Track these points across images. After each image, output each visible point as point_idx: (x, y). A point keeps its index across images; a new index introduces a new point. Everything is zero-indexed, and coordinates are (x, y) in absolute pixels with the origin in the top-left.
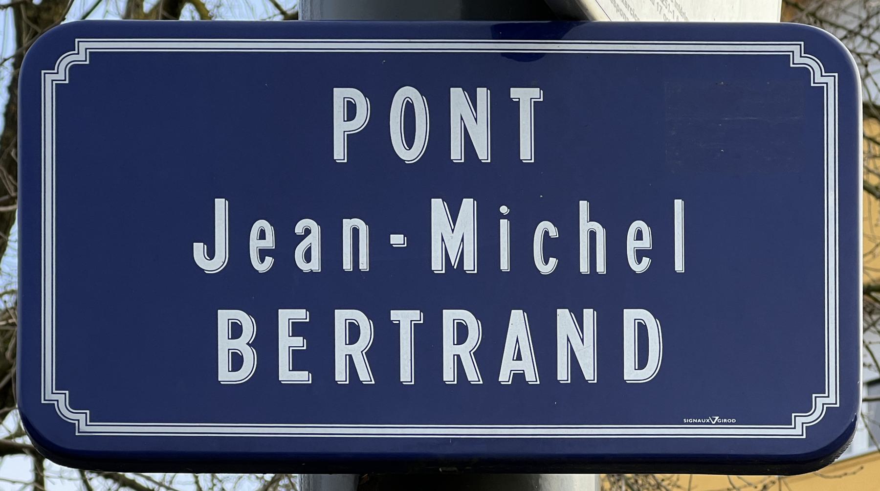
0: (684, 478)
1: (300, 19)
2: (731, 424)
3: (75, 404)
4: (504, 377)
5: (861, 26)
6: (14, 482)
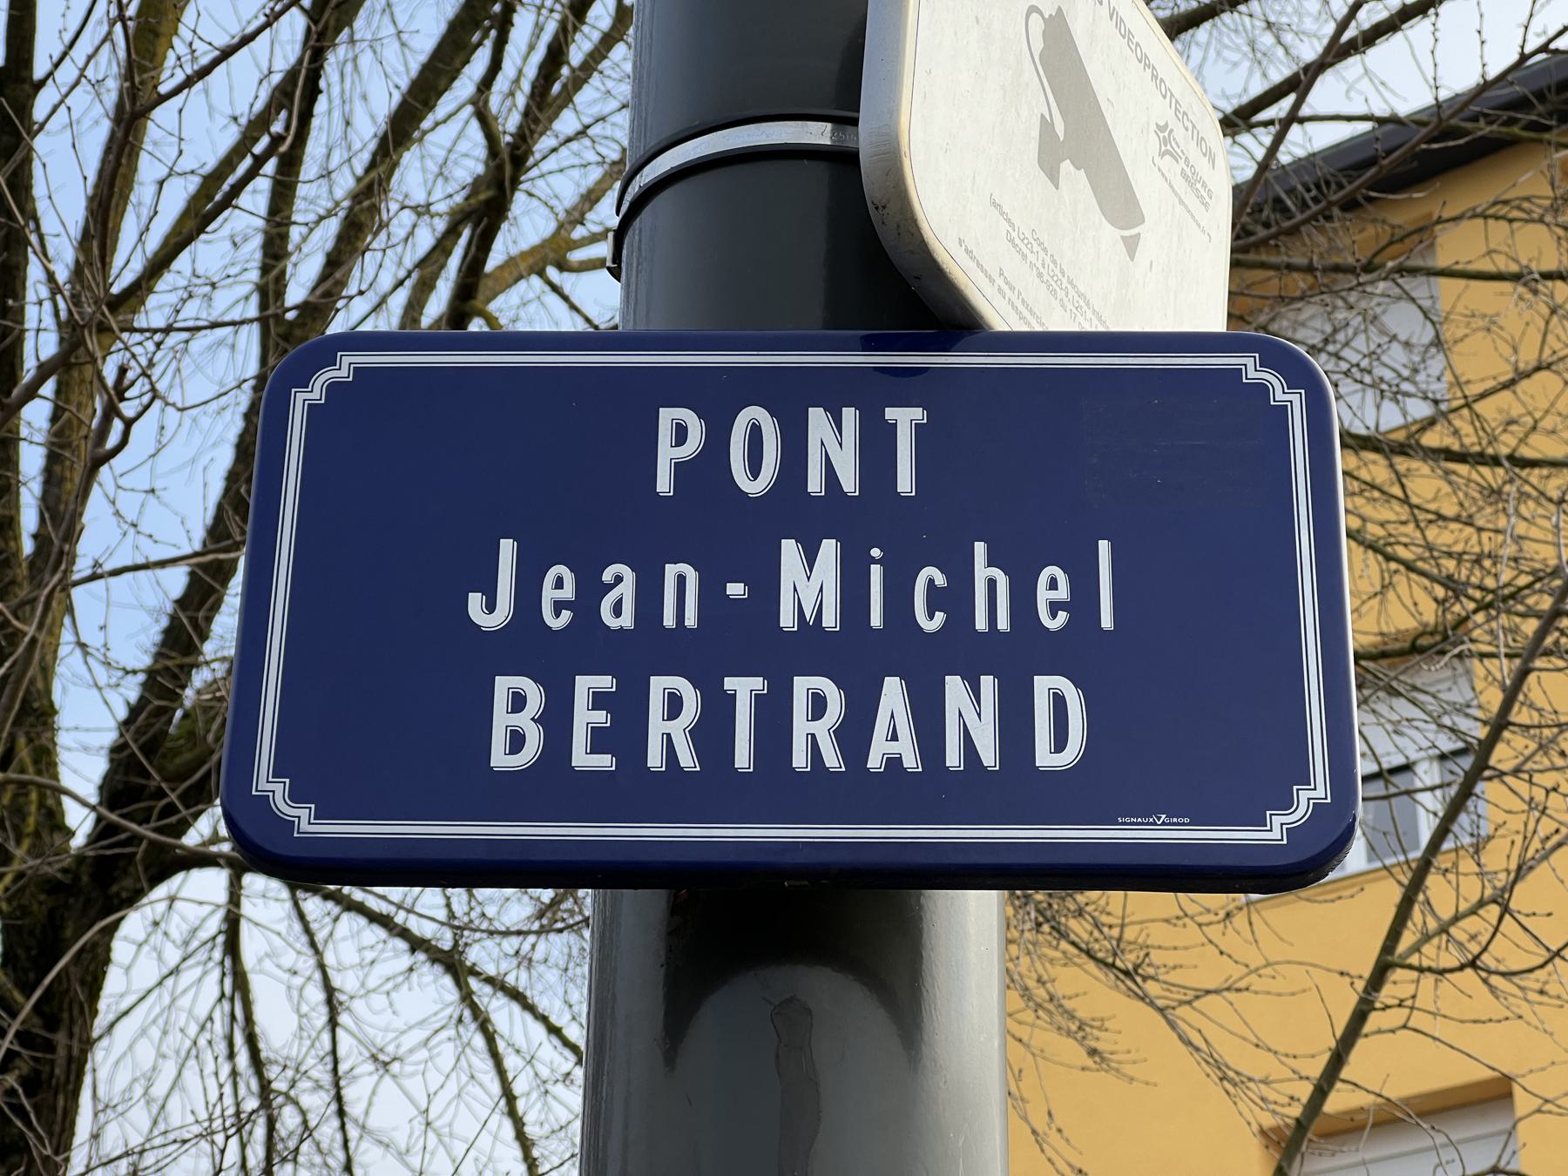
0: (1116, 896)
1: (620, 328)
2: (1184, 824)
3: (296, 796)
4: (875, 762)
5: (1326, 341)
6: (201, 903)
